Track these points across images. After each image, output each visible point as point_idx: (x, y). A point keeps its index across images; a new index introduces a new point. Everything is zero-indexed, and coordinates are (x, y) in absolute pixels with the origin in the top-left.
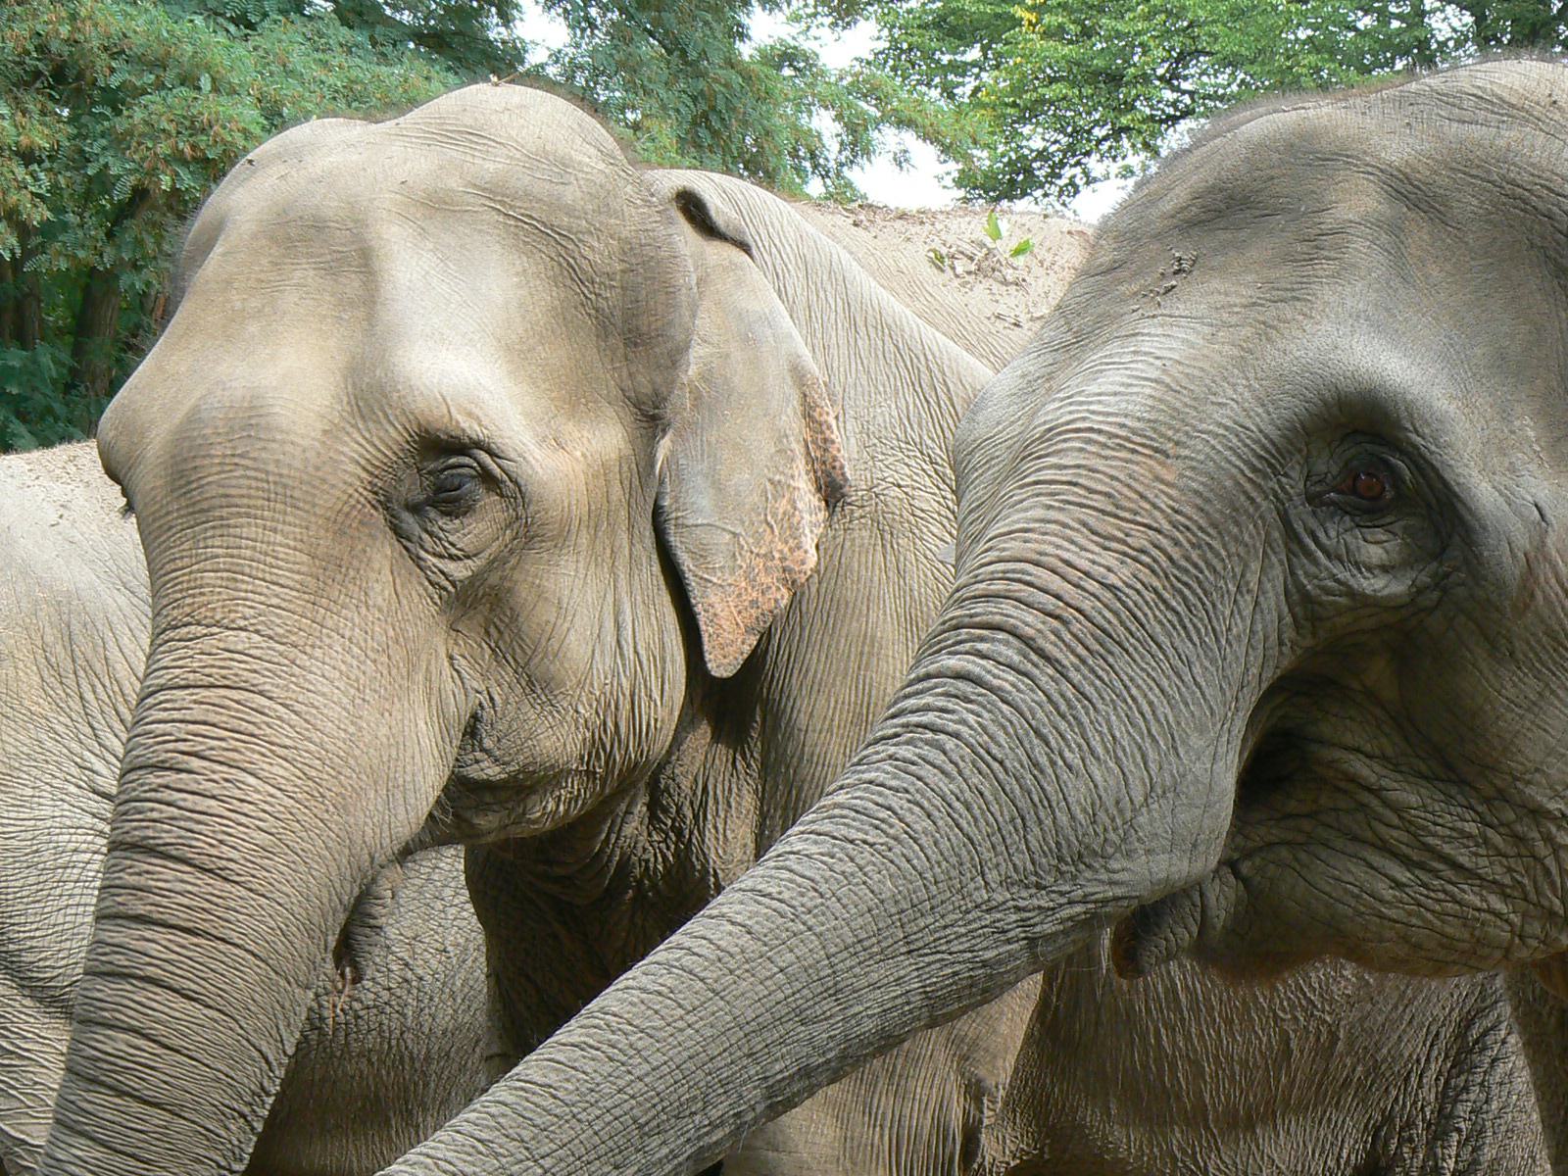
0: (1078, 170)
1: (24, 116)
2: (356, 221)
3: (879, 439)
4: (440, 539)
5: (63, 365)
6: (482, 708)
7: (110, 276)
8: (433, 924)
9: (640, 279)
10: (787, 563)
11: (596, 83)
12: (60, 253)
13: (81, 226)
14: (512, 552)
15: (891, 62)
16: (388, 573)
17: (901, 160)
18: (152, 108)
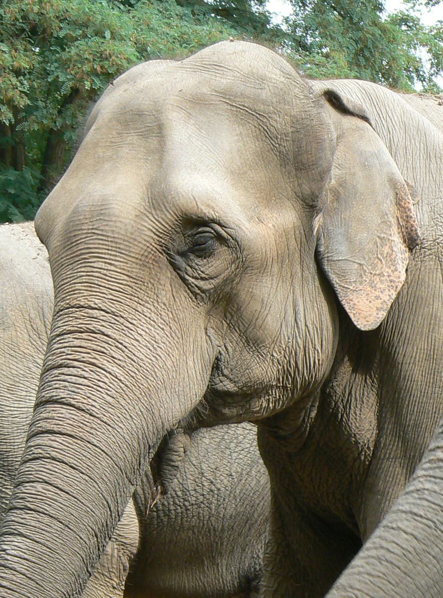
1: (16, 52)
2: (157, 111)
3: (439, 215)
4: (196, 269)
5: (37, 178)
6: (221, 354)
7: (60, 133)
8: (225, 462)
10: (391, 278)
11: (307, 34)
12: (34, 121)
13: (46, 107)
14: (236, 275)
16: (169, 286)
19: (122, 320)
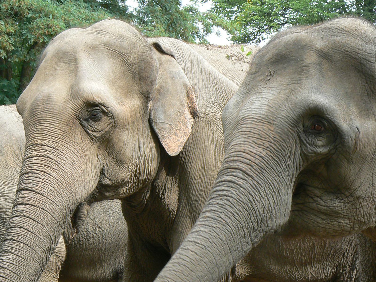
0: (260, 36)
2: (74, 52)
4: (92, 127)
5: (17, 84)
6: (104, 167)
7: (28, 63)
8: (106, 218)
9: (142, 64)
10: (185, 131)
11: (145, 16)
12: (16, 57)
13: (22, 51)
14: (111, 130)
15: (215, 11)
16: (80, 135)
17: (218, 34)
18: (38, 22)
19: (57, 151)
